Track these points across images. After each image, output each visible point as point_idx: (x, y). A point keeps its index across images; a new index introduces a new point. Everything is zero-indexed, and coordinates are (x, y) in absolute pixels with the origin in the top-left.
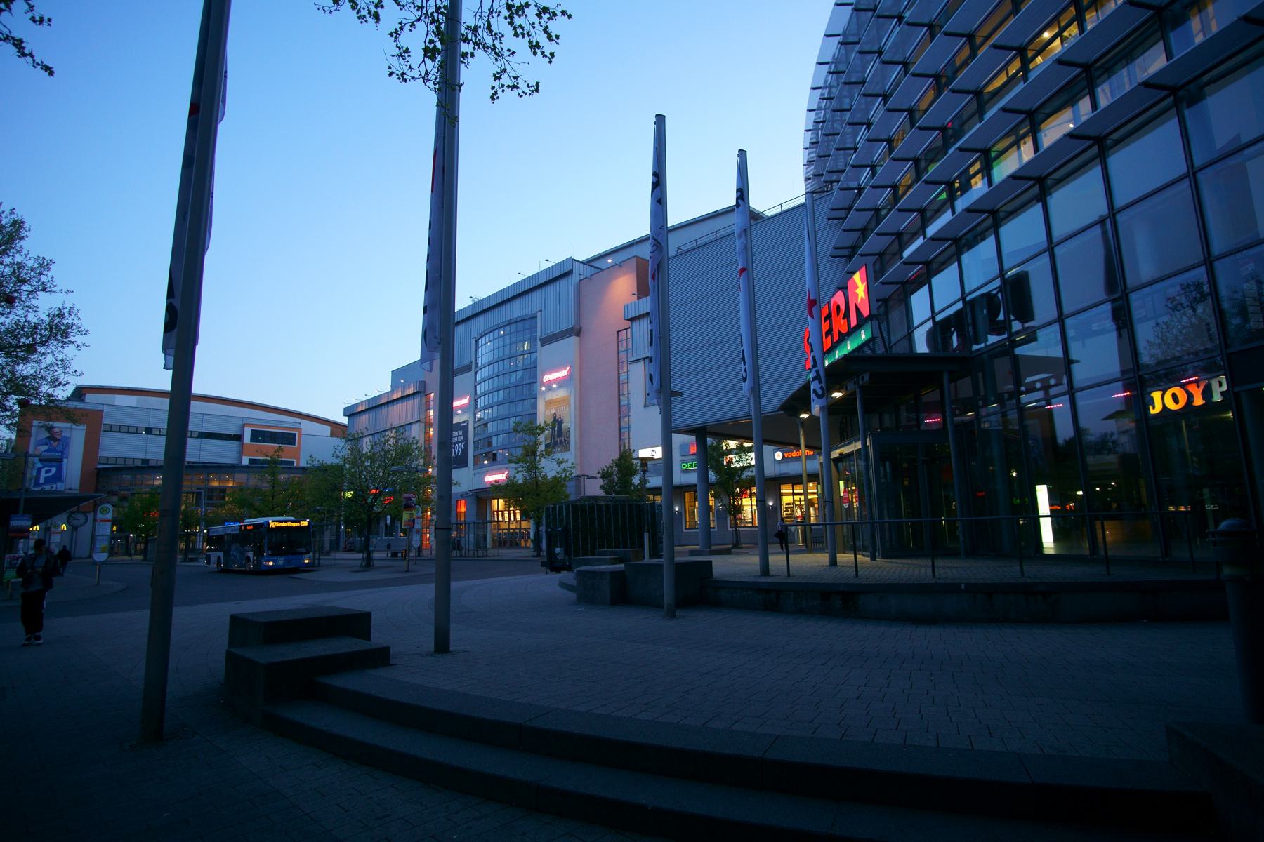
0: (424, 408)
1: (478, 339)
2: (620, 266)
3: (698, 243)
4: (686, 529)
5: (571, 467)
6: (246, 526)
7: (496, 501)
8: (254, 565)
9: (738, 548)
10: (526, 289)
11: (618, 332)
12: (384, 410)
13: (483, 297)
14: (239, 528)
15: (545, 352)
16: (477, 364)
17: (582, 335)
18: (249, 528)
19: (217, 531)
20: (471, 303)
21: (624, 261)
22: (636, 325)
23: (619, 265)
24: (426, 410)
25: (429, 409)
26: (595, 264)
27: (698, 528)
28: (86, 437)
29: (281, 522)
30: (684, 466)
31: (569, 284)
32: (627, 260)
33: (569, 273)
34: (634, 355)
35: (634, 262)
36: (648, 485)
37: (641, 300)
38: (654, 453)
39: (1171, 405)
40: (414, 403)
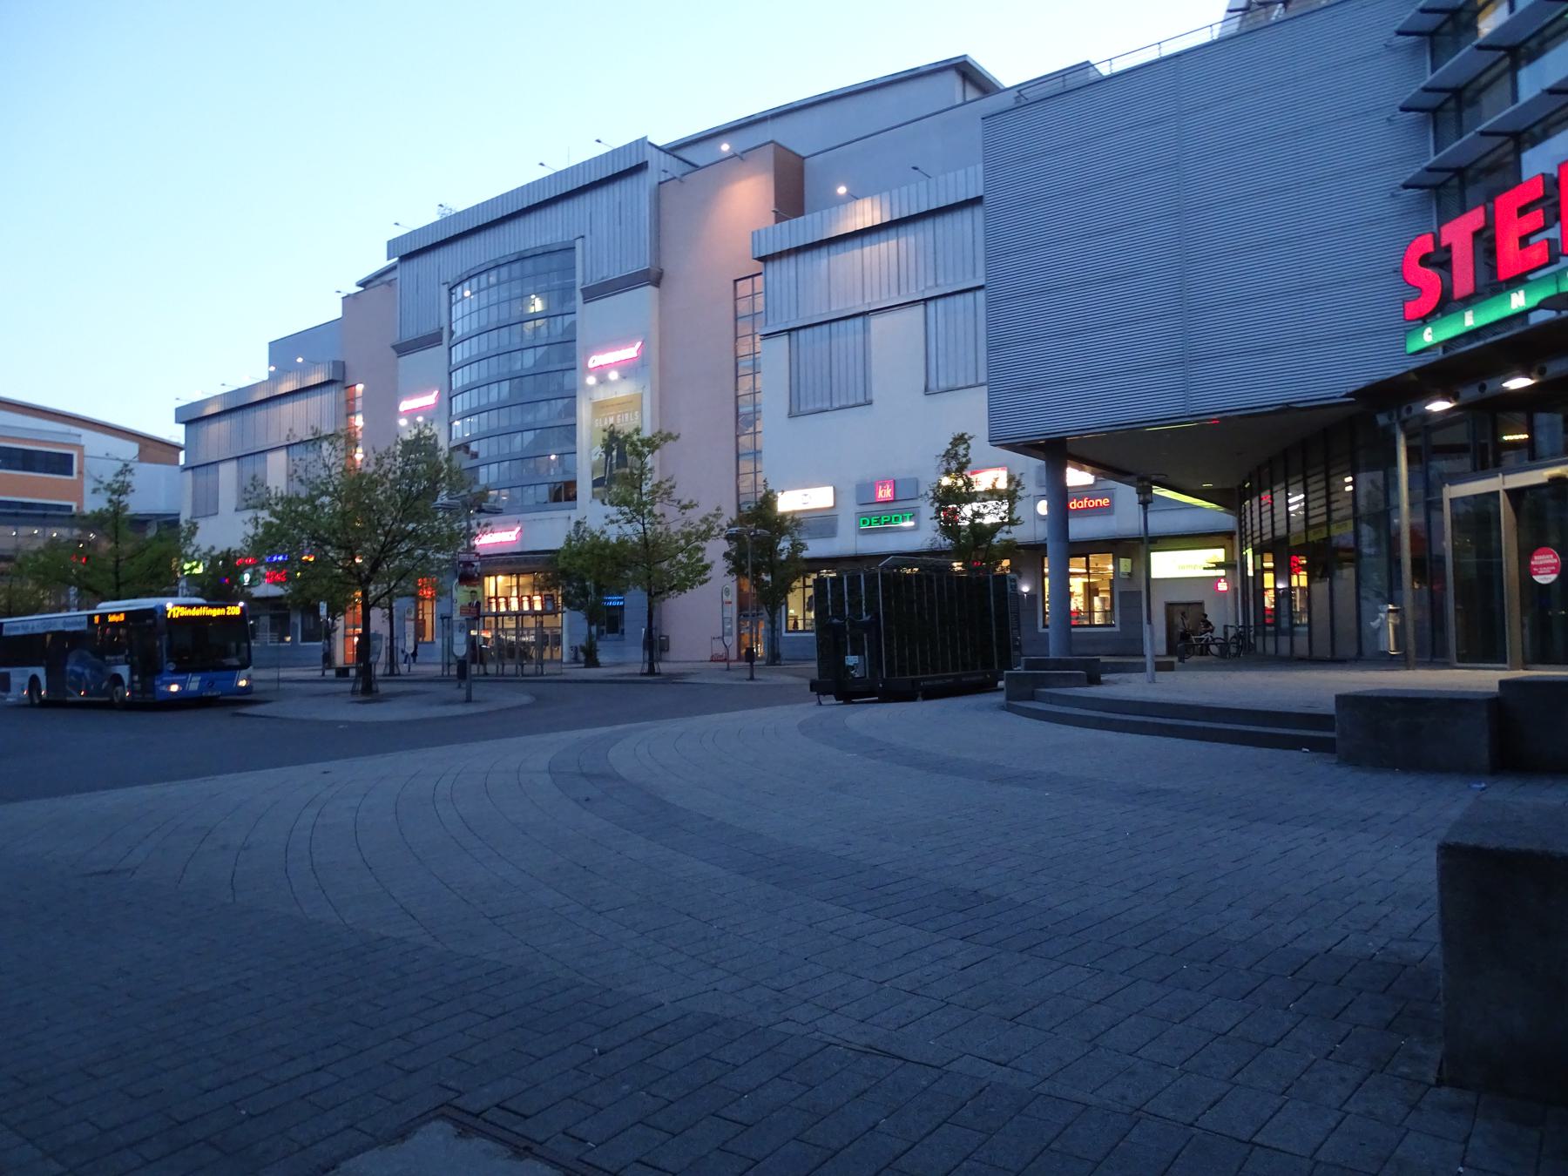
0: (344, 411)
1: (455, 286)
2: (742, 159)
3: (1067, 83)
4: (787, 631)
5: (715, 516)
6: (104, 617)
7: (492, 579)
8: (132, 692)
9: (775, 665)
10: (553, 195)
11: (736, 281)
12: (261, 414)
13: (460, 209)
14: (85, 619)
15: (589, 316)
16: (452, 333)
17: (664, 283)
18: (111, 619)
19: (23, 627)
20: (437, 218)
21: (750, 150)
22: (773, 269)
23: (738, 156)
24: (348, 415)
25: (354, 413)
26: (687, 154)
27: (1114, 626)
28: (468, 210)
29: (190, 606)
30: (864, 522)
31: (639, 191)
32: (755, 148)
33: (640, 168)
34: (770, 322)
35: (769, 151)
36: (805, 554)
37: (778, 225)
38: (806, 499)
39: (1100, 501)
40: (328, 398)
